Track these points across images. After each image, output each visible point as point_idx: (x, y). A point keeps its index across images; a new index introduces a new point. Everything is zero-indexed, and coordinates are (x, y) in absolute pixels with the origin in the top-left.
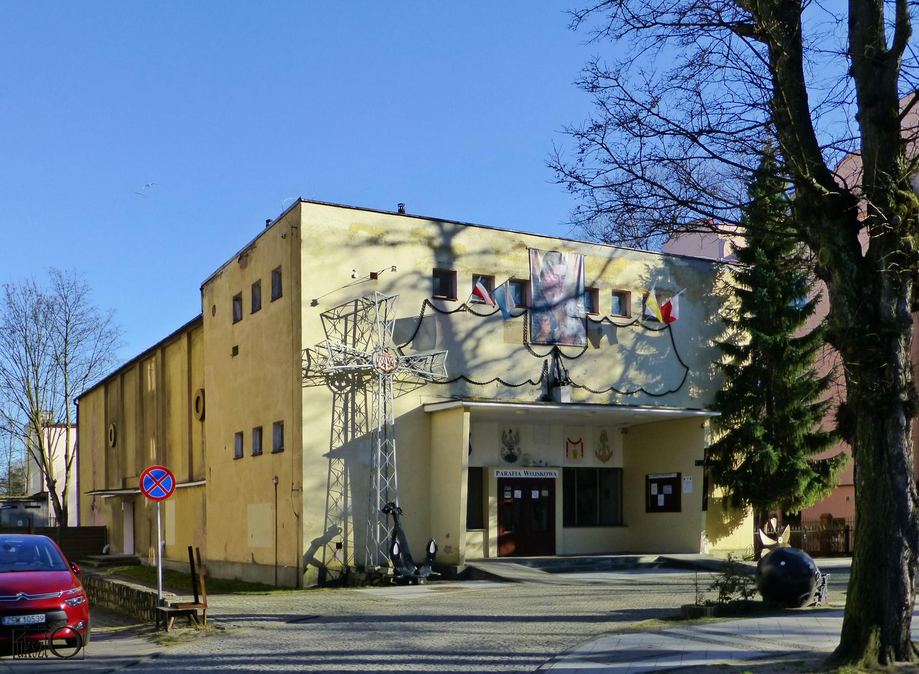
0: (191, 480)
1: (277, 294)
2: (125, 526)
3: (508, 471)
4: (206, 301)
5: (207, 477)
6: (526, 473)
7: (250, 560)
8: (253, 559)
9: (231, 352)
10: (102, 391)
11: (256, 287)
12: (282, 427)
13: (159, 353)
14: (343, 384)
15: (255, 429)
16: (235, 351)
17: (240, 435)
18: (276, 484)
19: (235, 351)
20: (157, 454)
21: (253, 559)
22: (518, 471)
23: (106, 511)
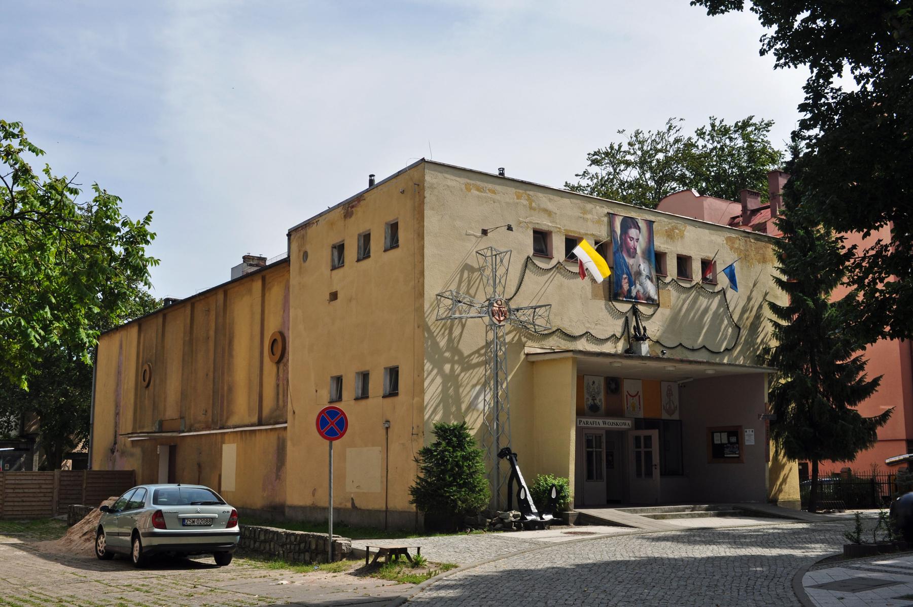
0: (260, 423)
1: (393, 243)
2: (160, 468)
3: (590, 420)
4: (294, 246)
5: (290, 417)
6: (604, 423)
7: (349, 505)
8: (353, 504)
9: (328, 297)
10: (134, 331)
11: (366, 238)
12: (397, 372)
13: (221, 296)
14: (502, 318)
15: (334, 247)
16: (334, 296)
17: (339, 380)
18: (387, 428)
19: (334, 296)
20: (797, 548)
21: (353, 504)
22: (597, 421)
23: (132, 455)
